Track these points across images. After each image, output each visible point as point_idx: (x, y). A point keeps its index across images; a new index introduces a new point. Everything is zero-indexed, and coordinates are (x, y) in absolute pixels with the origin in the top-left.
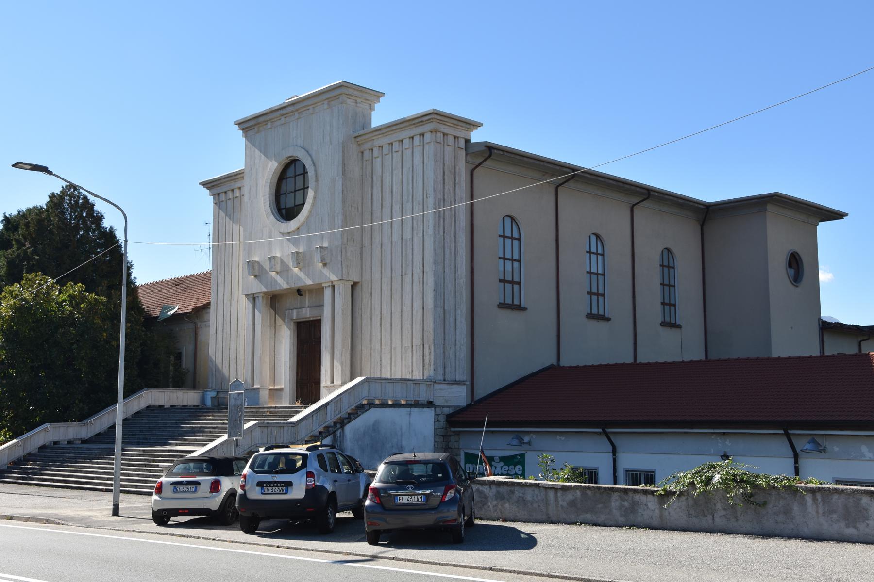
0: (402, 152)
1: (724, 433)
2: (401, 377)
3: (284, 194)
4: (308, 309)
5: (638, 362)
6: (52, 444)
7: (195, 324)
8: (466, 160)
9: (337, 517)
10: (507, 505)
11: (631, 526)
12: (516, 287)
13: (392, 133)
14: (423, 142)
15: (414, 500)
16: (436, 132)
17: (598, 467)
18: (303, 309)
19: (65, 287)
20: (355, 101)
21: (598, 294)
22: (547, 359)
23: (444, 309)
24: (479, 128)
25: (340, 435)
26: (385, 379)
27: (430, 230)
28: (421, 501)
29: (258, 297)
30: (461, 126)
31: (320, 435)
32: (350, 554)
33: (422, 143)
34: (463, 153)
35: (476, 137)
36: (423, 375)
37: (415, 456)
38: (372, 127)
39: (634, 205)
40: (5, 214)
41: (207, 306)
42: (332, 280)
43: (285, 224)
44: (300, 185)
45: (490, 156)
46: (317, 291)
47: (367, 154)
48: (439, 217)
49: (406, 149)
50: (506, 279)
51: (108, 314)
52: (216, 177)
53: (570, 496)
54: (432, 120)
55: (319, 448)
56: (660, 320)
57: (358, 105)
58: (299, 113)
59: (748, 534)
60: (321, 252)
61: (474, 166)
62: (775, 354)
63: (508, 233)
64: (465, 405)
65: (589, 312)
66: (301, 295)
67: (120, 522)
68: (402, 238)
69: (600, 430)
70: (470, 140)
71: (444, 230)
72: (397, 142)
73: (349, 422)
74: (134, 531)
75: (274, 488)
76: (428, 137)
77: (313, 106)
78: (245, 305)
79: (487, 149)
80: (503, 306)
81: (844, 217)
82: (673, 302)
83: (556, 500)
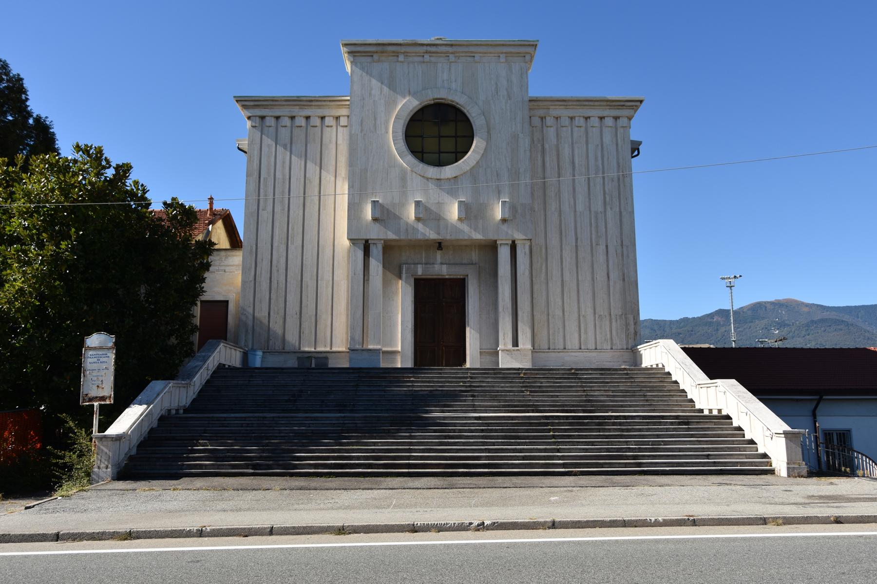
13: (578, 107)
17: (851, 429)
68: (590, 211)
77: (481, 55)
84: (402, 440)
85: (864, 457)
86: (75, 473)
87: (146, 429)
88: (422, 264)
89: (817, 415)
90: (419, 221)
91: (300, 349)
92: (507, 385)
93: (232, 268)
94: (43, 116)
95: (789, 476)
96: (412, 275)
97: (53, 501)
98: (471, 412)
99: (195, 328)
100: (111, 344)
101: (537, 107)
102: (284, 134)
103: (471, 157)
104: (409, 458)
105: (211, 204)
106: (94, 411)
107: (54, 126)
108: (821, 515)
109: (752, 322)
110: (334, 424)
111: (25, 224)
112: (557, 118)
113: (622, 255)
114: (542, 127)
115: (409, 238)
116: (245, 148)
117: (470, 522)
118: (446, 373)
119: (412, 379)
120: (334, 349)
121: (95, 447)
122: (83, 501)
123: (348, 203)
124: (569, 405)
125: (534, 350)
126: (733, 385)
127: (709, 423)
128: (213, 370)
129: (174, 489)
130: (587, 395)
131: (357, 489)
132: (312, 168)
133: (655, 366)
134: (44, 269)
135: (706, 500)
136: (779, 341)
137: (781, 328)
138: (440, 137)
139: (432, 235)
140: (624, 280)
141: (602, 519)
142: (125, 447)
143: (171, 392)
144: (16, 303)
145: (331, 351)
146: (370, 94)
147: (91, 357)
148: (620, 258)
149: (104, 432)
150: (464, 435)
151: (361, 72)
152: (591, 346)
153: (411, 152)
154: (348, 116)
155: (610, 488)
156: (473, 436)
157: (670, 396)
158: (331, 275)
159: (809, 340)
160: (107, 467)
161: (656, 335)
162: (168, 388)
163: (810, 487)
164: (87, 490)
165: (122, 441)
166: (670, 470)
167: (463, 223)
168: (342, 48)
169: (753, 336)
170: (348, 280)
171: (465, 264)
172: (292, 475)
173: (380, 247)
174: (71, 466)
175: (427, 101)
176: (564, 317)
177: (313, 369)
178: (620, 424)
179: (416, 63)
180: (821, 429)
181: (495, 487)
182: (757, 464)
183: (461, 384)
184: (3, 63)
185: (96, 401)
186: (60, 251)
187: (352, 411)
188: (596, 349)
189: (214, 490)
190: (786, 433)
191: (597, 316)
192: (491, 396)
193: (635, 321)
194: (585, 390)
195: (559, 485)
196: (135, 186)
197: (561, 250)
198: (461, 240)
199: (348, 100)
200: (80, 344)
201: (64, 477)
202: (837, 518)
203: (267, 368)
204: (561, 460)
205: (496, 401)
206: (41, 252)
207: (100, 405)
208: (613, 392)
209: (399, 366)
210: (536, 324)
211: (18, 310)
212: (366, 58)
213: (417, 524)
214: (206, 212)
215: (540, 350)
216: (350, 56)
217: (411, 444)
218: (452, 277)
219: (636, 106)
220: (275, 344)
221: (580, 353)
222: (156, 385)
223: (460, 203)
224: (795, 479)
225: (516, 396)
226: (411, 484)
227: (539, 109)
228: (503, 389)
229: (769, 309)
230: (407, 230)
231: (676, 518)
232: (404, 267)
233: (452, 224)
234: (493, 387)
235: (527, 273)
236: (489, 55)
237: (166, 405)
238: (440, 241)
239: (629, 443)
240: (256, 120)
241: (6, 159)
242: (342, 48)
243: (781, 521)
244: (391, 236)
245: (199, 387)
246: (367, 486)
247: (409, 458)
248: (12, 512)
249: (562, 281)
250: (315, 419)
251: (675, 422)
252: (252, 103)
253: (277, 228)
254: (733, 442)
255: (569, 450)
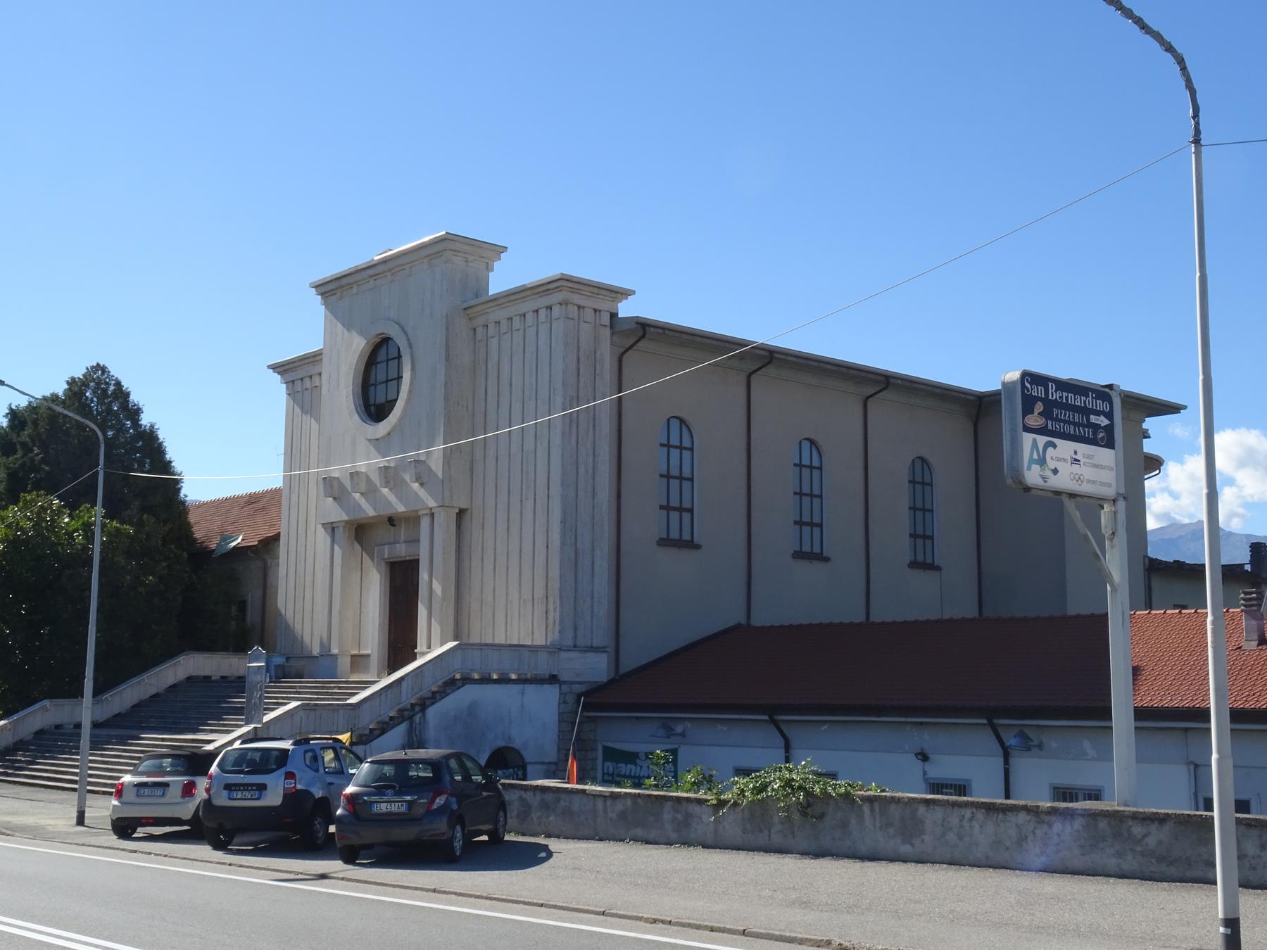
0: (525, 331)
1: (922, 723)
2: (481, 640)
3: (373, 385)
4: (404, 545)
5: (872, 619)
6: (53, 728)
7: (265, 562)
8: (611, 342)
9: (330, 831)
10: (552, 818)
11: (687, 843)
12: (686, 516)
14: (551, 319)
15: (394, 808)
16: (567, 304)
18: (398, 545)
19: (78, 511)
20: (465, 259)
21: (812, 524)
22: (734, 616)
23: (576, 548)
24: (629, 297)
25: (420, 722)
26: (486, 645)
27: (557, 440)
28: (403, 809)
29: (338, 527)
30: (603, 295)
31: (391, 721)
32: (301, 873)
33: (549, 320)
34: (608, 331)
35: (626, 309)
36: (546, 640)
37: (405, 754)
38: (490, 294)
39: (868, 398)
40: (10, 405)
41: (276, 538)
42: (430, 506)
43: (373, 427)
44: (393, 374)
45: (643, 336)
46: (412, 520)
47: (480, 330)
48: (571, 421)
49: (529, 327)
50: (671, 505)
51: (137, 548)
52: (282, 360)
53: (619, 806)
54: (560, 289)
55: (311, 742)
56: (908, 558)
57: (470, 264)
58: (392, 274)
59: (804, 853)
60: (415, 467)
61: (622, 350)
62: (1072, 611)
63: (675, 441)
64: (606, 681)
65: (798, 549)
66: (394, 525)
67: (81, 833)
68: (522, 450)
69: (766, 717)
70: (617, 314)
71: (578, 438)
72: (518, 317)
73: (433, 703)
74: (83, 845)
75: (244, 793)
76: (556, 310)
78: (322, 537)
79: (639, 326)
80: (665, 542)
81: (1181, 411)
82: (929, 533)
83: (605, 811)
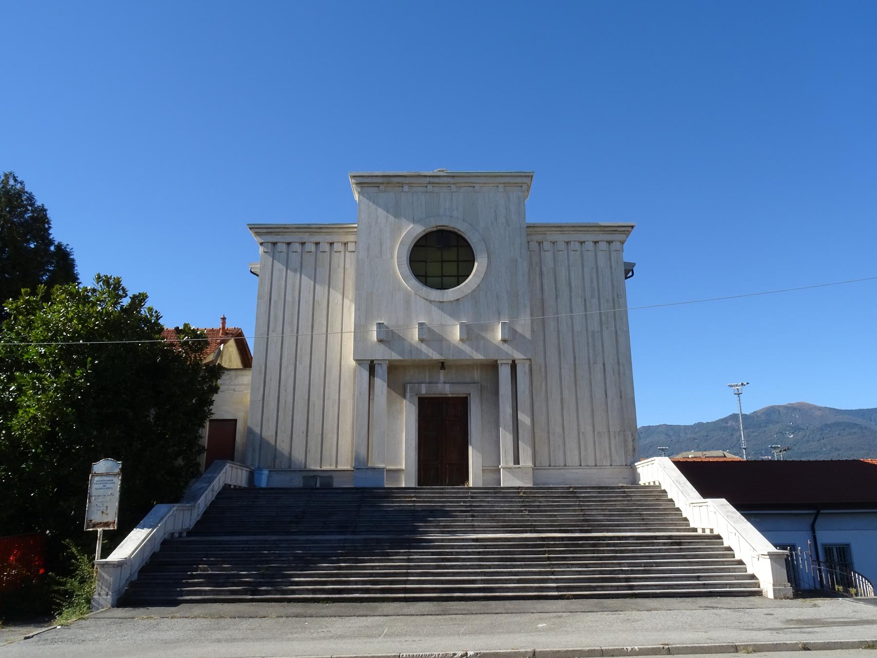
13: (574, 232)
68: (587, 330)
77: (481, 185)
84: (397, 561)
85: (856, 574)
86: (75, 600)
87: (148, 554)
88: (426, 383)
89: (816, 529)
90: (422, 342)
91: (305, 467)
92: (507, 504)
93: (241, 387)
94: (64, 243)
95: (775, 598)
96: (416, 394)
97: (52, 630)
98: (470, 532)
99: (202, 449)
100: (117, 470)
101: (534, 233)
102: (295, 258)
103: (479, 267)
104: (406, 582)
105: (224, 323)
106: (97, 537)
107: (75, 253)
108: (790, 642)
109: (766, 426)
110: (334, 547)
111: (41, 352)
112: (554, 243)
113: (619, 374)
114: (540, 251)
115: (413, 358)
116: (257, 271)
117: (454, 652)
118: (448, 493)
119: (413, 499)
120: (340, 468)
121: (97, 574)
122: (81, 631)
123: (354, 325)
124: (566, 525)
125: (535, 468)
126: (723, 505)
127: (700, 544)
128: (218, 491)
129: (172, 618)
130: (585, 514)
131: (352, 616)
132: (321, 290)
133: (652, 484)
134: (58, 396)
135: (687, 626)
136: (783, 450)
137: (796, 433)
138: (443, 261)
139: (435, 356)
140: (621, 397)
141: (581, 649)
142: (126, 574)
143: (175, 515)
144: (29, 430)
145: (336, 469)
146: (376, 222)
147: (98, 483)
148: (617, 376)
149: (106, 558)
150: (460, 558)
151: (368, 201)
152: (591, 462)
153: (415, 276)
154: (356, 242)
155: (598, 613)
156: (469, 558)
157: (666, 515)
158: (337, 394)
159: (824, 444)
160: (107, 595)
161: (672, 441)
162: (172, 511)
163: (792, 610)
164: (86, 619)
165: (123, 567)
166: (660, 593)
167: (465, 343)
168: (350, 179)
169: (768, 441)
170: (354, 399)
171: (467, 383)
172: (290, 601)
173: (385, 367)
174: (72, 593)
175: (430, 228)
176: (564, 435)
177: (318, 489)
178: (614, 545)
179: (420, 193)
180: (821, 544)
181: (487, 613)
182: (746, 585)
183: (462, 504)
184: (30, 195)
185: (100, 527)
186: (75, 379)
187: (353, 533)
188: (596, 466)
189: (211, 618)
190: (771, 555)
191: (596, 434)
192: (490, 516)
193: (633, 438)
194: (582, 509)
195: (550, 610)
196: (149, 313)
197: (560, 369)
198: (463, 360)
199: (356, 227)
200: (88, 470)
201: (64, 604)
202: (805, 644)
203: (272, 489)
204: (556, 583)
205: (495, 521)
206: (57, 380)
207: (104, 531)
208: (610, 510)
209: (404, 486)
210: (537, 441)
211: (30, 437)
212: (372, 188)
213: (403, 655)
214: (218, 331)
215: (541, 468)
216: (358, 187)
217: (409, 567)
218: (454, 396)
219: (628, 231)
220: (281, 462)
221: (581, 470)
222: (160, 509)
223: (462, 325)
224: (781, 601)
225: (515, 516)
226: (406, 610)
227: (536, 234)
228: (502, 509)
229: (782, 413)
230: (411, 351)
231: (652, 647)
232: (408, 386)
233: (454, 345)
234: (493, 506)
235: (527, 392)
236: (489, 185)
237: (170, 528)
238: (443, 361)
239: (621, 565)
240: (268, 246)
241: (29, 289)
242: (350, 179)
243: (751, 649)
244: (395, 356)
245: (204, 508)
246: (361, 613)
247: (406, 582)
248: (11, 643)
249: (562, 398)
250: (316, 542)
251: (668, 543)
252: (265, 231)
253: (286, 349)
254: (723, 563)
255: (563, 573)
